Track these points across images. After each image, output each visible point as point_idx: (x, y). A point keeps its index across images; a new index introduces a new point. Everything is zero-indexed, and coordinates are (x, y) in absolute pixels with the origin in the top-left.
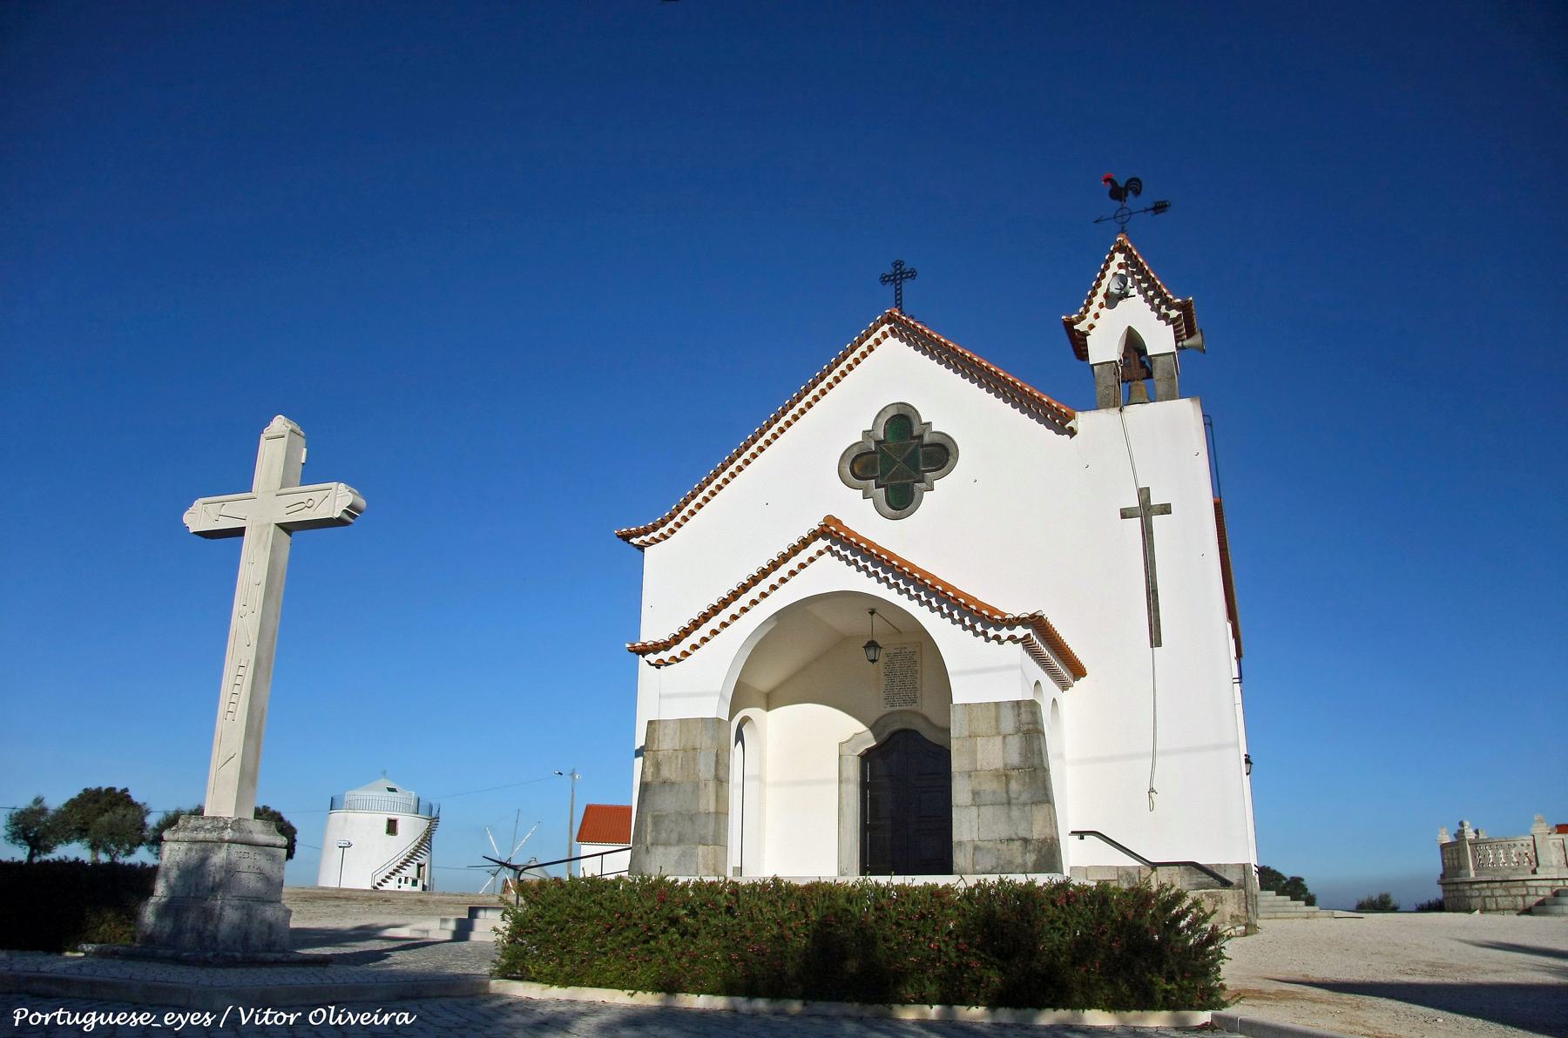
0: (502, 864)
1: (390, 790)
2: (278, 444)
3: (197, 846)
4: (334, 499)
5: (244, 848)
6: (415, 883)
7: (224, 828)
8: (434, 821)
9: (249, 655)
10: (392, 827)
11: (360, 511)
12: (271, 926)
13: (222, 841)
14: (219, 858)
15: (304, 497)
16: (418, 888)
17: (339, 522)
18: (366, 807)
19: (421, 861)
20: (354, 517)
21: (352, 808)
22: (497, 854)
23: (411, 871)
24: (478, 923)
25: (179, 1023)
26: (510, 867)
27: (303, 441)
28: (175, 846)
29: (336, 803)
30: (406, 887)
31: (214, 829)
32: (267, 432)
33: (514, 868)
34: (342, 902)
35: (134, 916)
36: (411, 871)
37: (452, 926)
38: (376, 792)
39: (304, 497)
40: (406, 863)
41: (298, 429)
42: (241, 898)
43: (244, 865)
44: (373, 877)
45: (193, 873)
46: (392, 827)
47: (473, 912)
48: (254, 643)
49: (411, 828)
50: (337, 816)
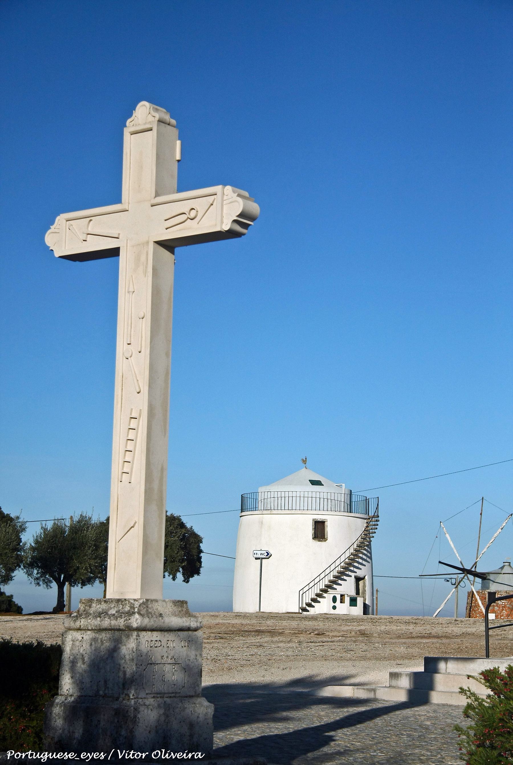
0: (464, 571)
1: (314, 483)
2: (145, 140)
3: (104, 636)
4: (219, 207)
5: (156, 636)
6: (353, 602)
7: (130, 613)
8: (372, 521)
9: (141, 404)
10: (319, 531)
11: (253, 218)
12: (191, 725)
13: (130, 629)
14: (129, 646)
15: (184, 207)
16: (357, 611)
17: (230, 234)
18: (285, 506)
19: (360, 573)
20: (246, 226)
21: (269, 510)
22: (457, 560)
23: (347, 587)
24: (440, 680)
25: (88, 757)
26: (476, 575)
27: (175, 132)
28: (78, 635)
29: (249, 503)
30: (343, 609)
31: (120, 614)
32: (131, 125)
33: (483, 576)
34: (267, 638)
35: (46, 718)
36: (347, 587)
37: (405, 683)
38: (297, 486)
39: (184, 207)
40: (340, 576)
41: (167, 117)
42: (159, 695)
43: (158, 654)
44: (301, 596)
45: (104, 664)
46: (319, 531)
47: (431, 664)
48: (145, 390)
49: (345, 533)
50: (250, 519)
